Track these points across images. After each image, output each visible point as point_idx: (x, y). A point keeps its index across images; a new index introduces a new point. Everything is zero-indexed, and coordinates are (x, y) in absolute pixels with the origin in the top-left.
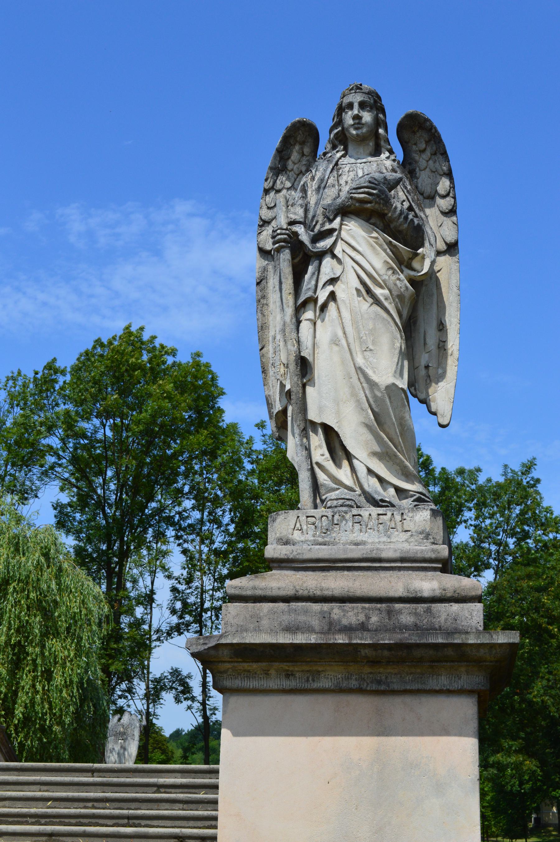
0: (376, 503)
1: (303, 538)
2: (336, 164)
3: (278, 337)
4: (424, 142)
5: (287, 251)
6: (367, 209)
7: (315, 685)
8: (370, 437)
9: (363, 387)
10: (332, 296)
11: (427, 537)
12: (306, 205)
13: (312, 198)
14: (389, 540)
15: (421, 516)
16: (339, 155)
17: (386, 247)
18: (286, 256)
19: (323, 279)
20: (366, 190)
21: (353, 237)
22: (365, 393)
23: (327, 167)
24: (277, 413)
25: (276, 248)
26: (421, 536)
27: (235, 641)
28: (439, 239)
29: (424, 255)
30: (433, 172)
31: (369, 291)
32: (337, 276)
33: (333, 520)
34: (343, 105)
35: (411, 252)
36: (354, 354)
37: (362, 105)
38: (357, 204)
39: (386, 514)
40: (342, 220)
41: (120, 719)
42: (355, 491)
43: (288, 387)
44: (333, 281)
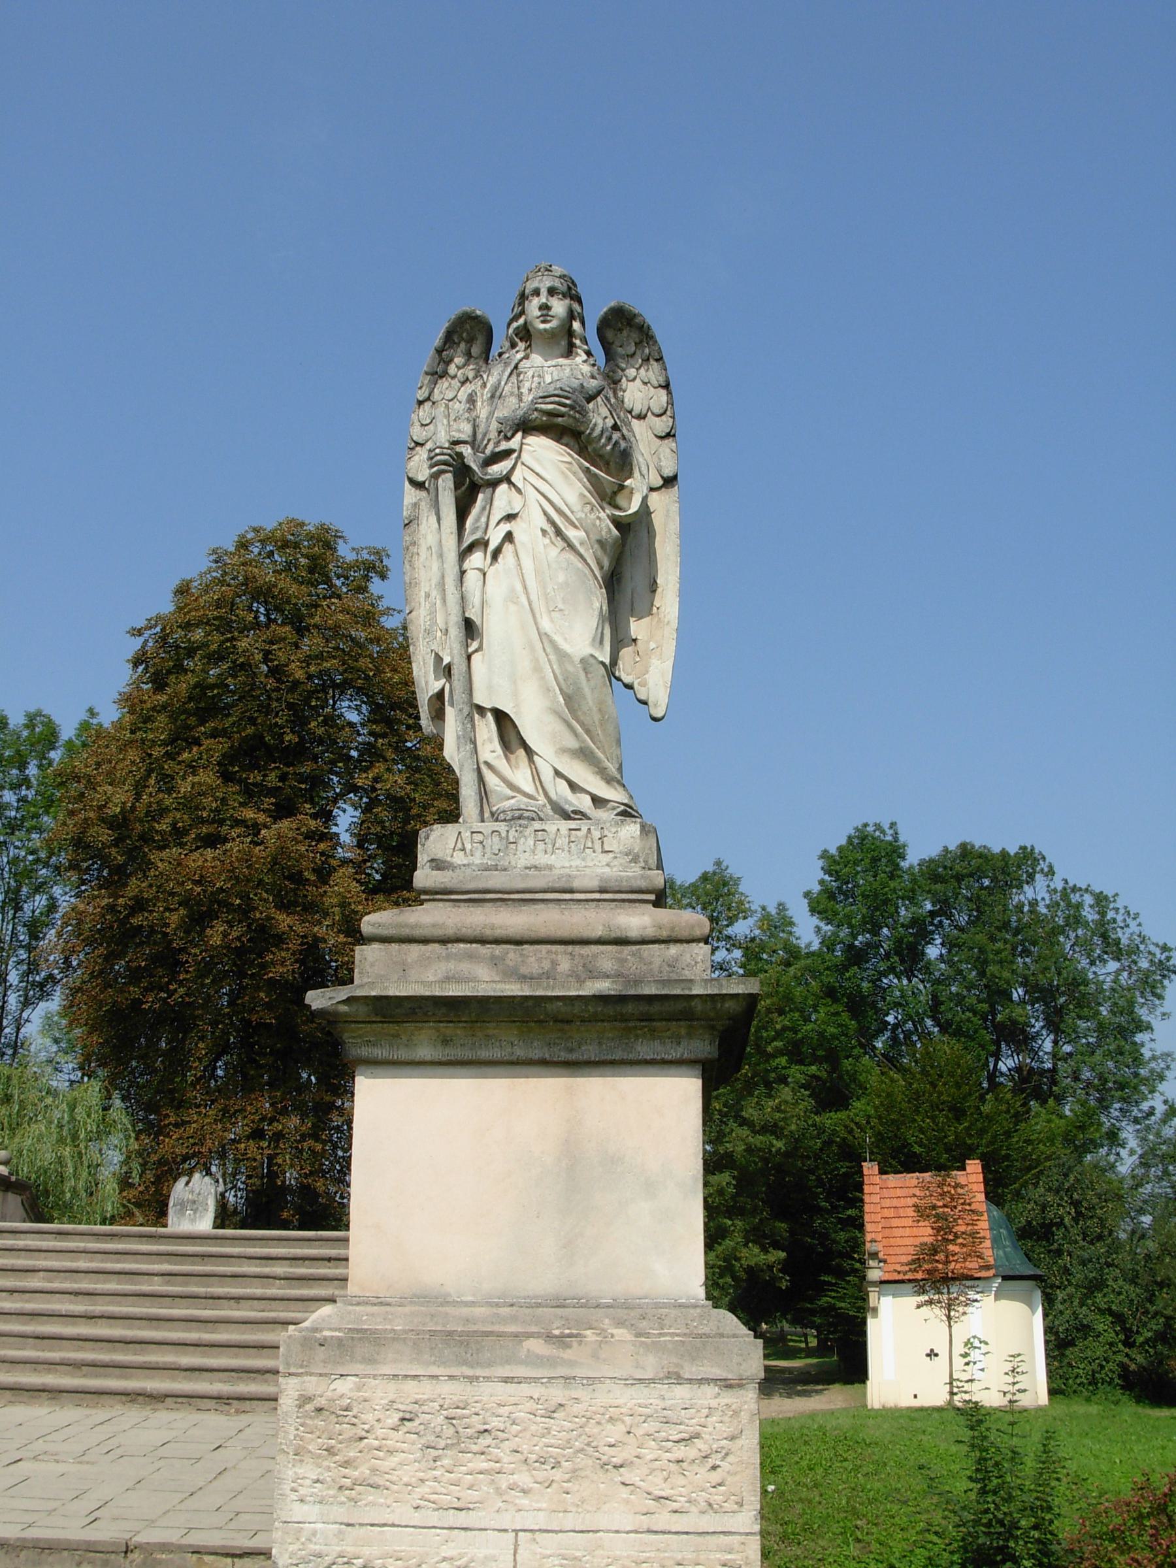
0: (566, 816)
1: (465, 862)
2: (516, 367)
3: (434, 593)
5: (449, 476)
6: (557, 425)
8: (560, 727)
9: (549, 660)
10: (509, 537)
11: (635, 860)
12: (474, 420)
13: (482, 410)
14: (583, 864)
16: (520, 356)
17: (582, 475)
18: (447, 482)
19: (497, 515)
21: (537, 460)
22: (552, 668)
23: (503, 372)
25: (434, 473)
26: (627, 859)
28: (653, 472)
29: (632, 489)
30: (645, 384)
31: (559, 532)
32: (516, 511)
33: (507, 836)
34: (527, 291)
36: (538, 616)
37: (552, 291)
38: (544, 419)
40: (523, 438)
41: (187, 1183)
43: (446, 660)
44: (510, 517)
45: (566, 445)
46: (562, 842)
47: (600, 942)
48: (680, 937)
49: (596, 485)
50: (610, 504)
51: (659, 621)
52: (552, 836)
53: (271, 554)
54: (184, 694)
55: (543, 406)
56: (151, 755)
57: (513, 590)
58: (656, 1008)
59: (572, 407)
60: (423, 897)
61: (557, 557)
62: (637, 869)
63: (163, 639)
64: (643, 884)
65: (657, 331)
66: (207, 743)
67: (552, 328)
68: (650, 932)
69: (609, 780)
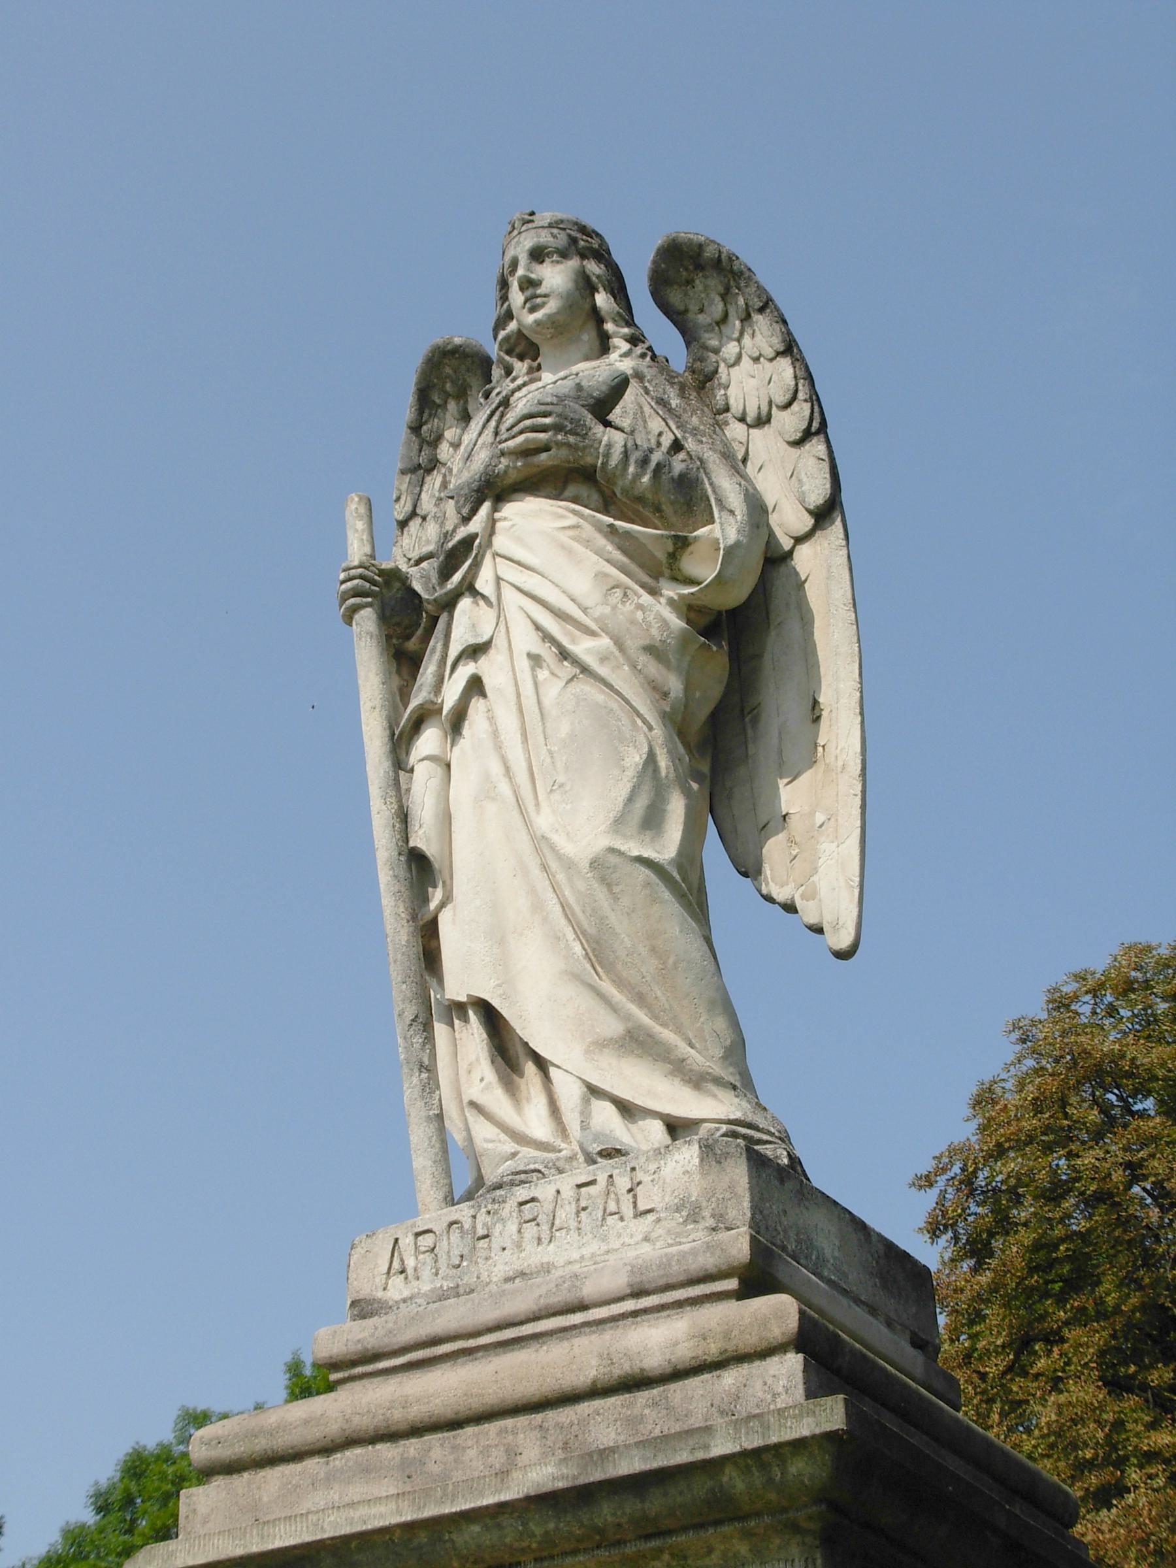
4: (718, 299)
8: (587, 1002)
10: (476, 686)
11: (694, 1217)
14: (604, 1248)
20: (528, 422)
21: (519, 540)
31: (564, 655)
32: (485, 638)
33: (474, 1227)
35: (668, 537)
39: (592, 1183)
42: (560, 1151)
44: (475, 651)
45: (575, 500)
46: (565, 1214)
47: (597, 1391)
48: (743, 1349)
50: (675, 579)
51: (828, 769)
52: (548, 1207)
53: (1112, 1011)
54: (1020, 1263)
56: (986, 1373)
57: (487, 777)
58: (655, 1503)
59: (557, 428)
60: (334, 1377)
61: (560, 695)
62: (700, 1234)
63: (968, 1182)
64: (709, 1262)
65: (748, 255)
66: (1072, 1334)
67: (549, 316)
68: (685, 1353)
69: (698, 1081)
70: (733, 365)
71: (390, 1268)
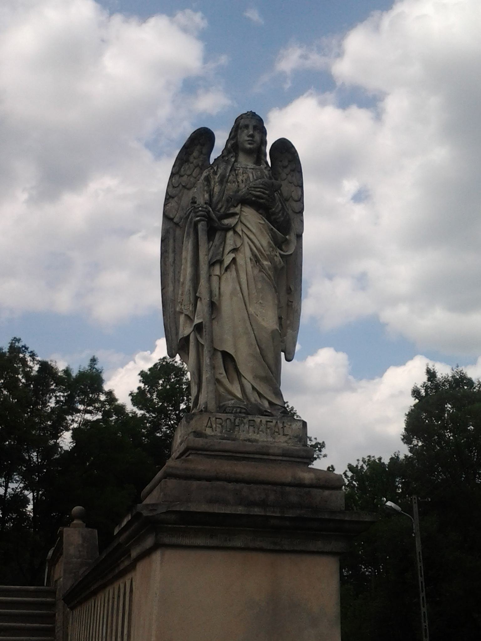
1: (213, 434)
7: (230, 544)
10: (234, 260)
14: (274, 441)
15: (296, 425)
20: (262, 190)
24: (181, 339)
26: (296, 440)
27: (182, 509)
32: (238, 247)
39: (272, 422)
46: (263, 427)
49: (274, 238)
55: (254, 192)
70: (283, 180)
71: (207, 425)
